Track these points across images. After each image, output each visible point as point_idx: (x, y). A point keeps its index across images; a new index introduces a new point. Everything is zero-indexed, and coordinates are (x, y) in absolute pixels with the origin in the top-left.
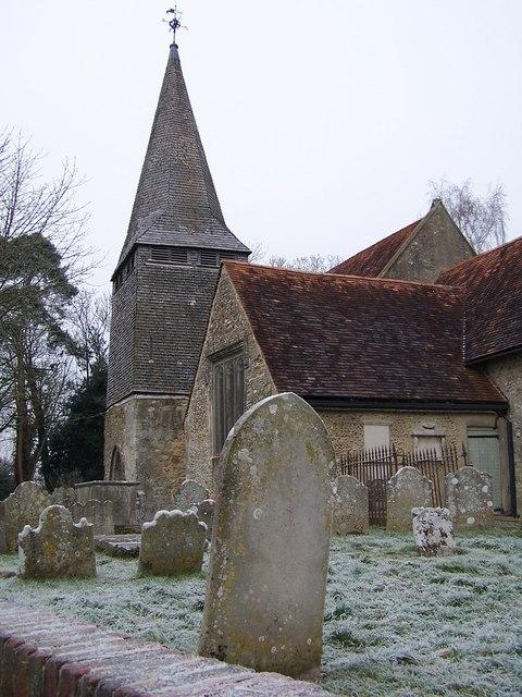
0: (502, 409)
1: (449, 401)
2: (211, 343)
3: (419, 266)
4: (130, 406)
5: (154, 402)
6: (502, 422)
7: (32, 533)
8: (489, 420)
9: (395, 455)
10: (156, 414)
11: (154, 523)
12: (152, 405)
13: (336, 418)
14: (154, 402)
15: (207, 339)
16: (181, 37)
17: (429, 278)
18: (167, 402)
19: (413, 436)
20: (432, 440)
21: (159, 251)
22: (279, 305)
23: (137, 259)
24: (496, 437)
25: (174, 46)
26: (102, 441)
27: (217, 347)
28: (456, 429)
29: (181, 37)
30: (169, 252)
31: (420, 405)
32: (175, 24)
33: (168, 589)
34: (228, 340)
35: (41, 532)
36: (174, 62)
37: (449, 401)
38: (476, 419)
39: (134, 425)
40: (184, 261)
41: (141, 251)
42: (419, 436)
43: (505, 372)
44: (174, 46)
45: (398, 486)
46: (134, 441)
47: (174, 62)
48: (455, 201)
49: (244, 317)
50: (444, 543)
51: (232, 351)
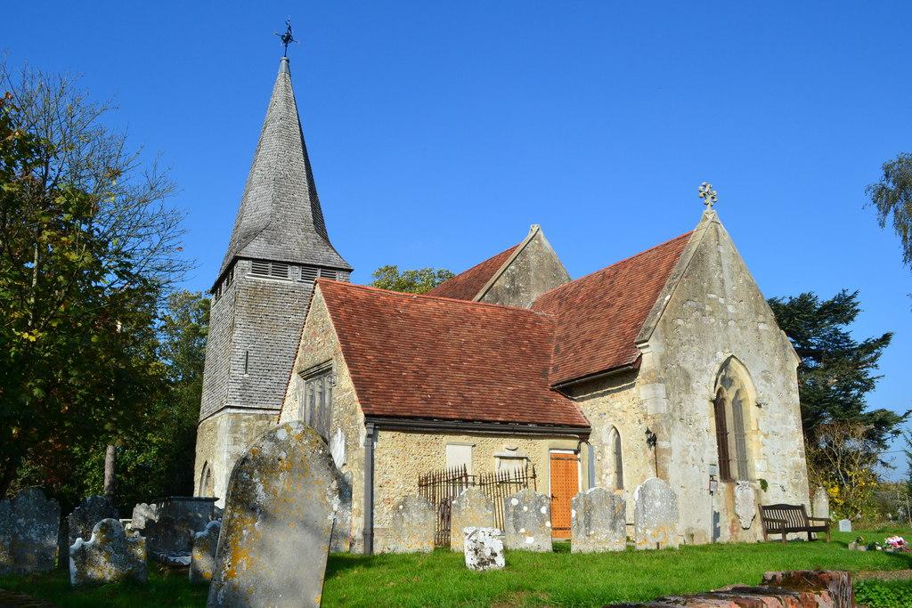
2: (306, 360)
3: (515, 292)
4: (223, 420)
5: (247, 417)
9: (466, 475)
10: (249, 429)
14: (247, 417)
15: (299, 355)
17: (529, 300)
18: (261, 417)
20: (514, 461)
23: (237, 270)
26: (194, 456)
27: (307, 364)
31: (504, 427)
33: (754, 428)
34: (320, 358)
39: (226, 440)
42: (501, 458)
48: (872, 373)
49: (334, 336)
50: (493, 561)
51: (319, 372)
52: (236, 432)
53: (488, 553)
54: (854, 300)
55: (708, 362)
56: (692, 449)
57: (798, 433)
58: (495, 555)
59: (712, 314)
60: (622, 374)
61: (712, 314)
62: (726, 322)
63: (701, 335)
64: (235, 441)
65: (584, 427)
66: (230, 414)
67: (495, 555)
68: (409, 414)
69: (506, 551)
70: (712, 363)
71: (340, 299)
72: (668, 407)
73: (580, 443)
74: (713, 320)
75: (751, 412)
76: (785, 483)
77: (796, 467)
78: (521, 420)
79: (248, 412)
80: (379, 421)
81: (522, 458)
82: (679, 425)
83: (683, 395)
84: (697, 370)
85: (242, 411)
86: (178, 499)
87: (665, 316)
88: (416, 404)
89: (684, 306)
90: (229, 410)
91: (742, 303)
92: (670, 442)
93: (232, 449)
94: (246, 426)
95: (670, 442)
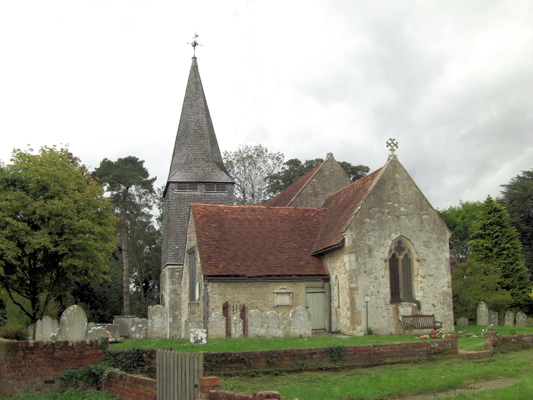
0: (326, 278)
1: (295, 275)
6: (326, 284)
7: (54, 336)
8: (320, 284)
11: (91, 331)
12: (178, 271)
13: (232, 285)
16: (199, 52)
19: (274, 293)
20: (285, 295)
21: (181, 185)
22: (215, 227)
23: (170, 189)
24: (324, 292)
25: (195, 58)
28: (301, 288)
29: (199, 52)
30: (187, 185)
32: (195, 44)
35: (57, 335)
36: (195, 69)
37: (295, 275)
38: (311, 284)
40: (196, 189)
41: (171, 185)
42: (277, 293)
43: (329, 259)
44: (195, 58)
45: (213, 319)
46: (168, 291)
47: (195, 69)
50: (202, 342)
52: (173, 278)
53: (199, 338)
54: (506, 191)
55: (385, 239)
56: (371, 287)
57: (447, 274)
58: (203, 339)
59: (389, 213)
60: (339, 248)
61: (389, 213)
62: (398, 217)
63: (382, 225)
64: (172, 283)
65: (326, 275)
66: (169, 268)
67: (202, 339)
68: (226, 274)
69: (207, 338)
70: (388, 240)
71: (202, 214)
72: (357, 266)
73: (324, 283)
74: (390, 217)
75: (416, 265)
76: (435, 302)
77: (445, 294)
78: (288, 274)
79: (179, 267)
80: (210, 278)
81: (290, 293)
82: (364, 275)
83: (367, 259)
84: (378, 245)
85: (176, 267)
86: (118, 317)
87: (357, 218)
88: (232, 269)
89: (371, 211)
90: (168, 267)
91: (411, 205)
92: (357, 284)
93: (171, 287)
94: (178, 275)
95: (357, 284)
